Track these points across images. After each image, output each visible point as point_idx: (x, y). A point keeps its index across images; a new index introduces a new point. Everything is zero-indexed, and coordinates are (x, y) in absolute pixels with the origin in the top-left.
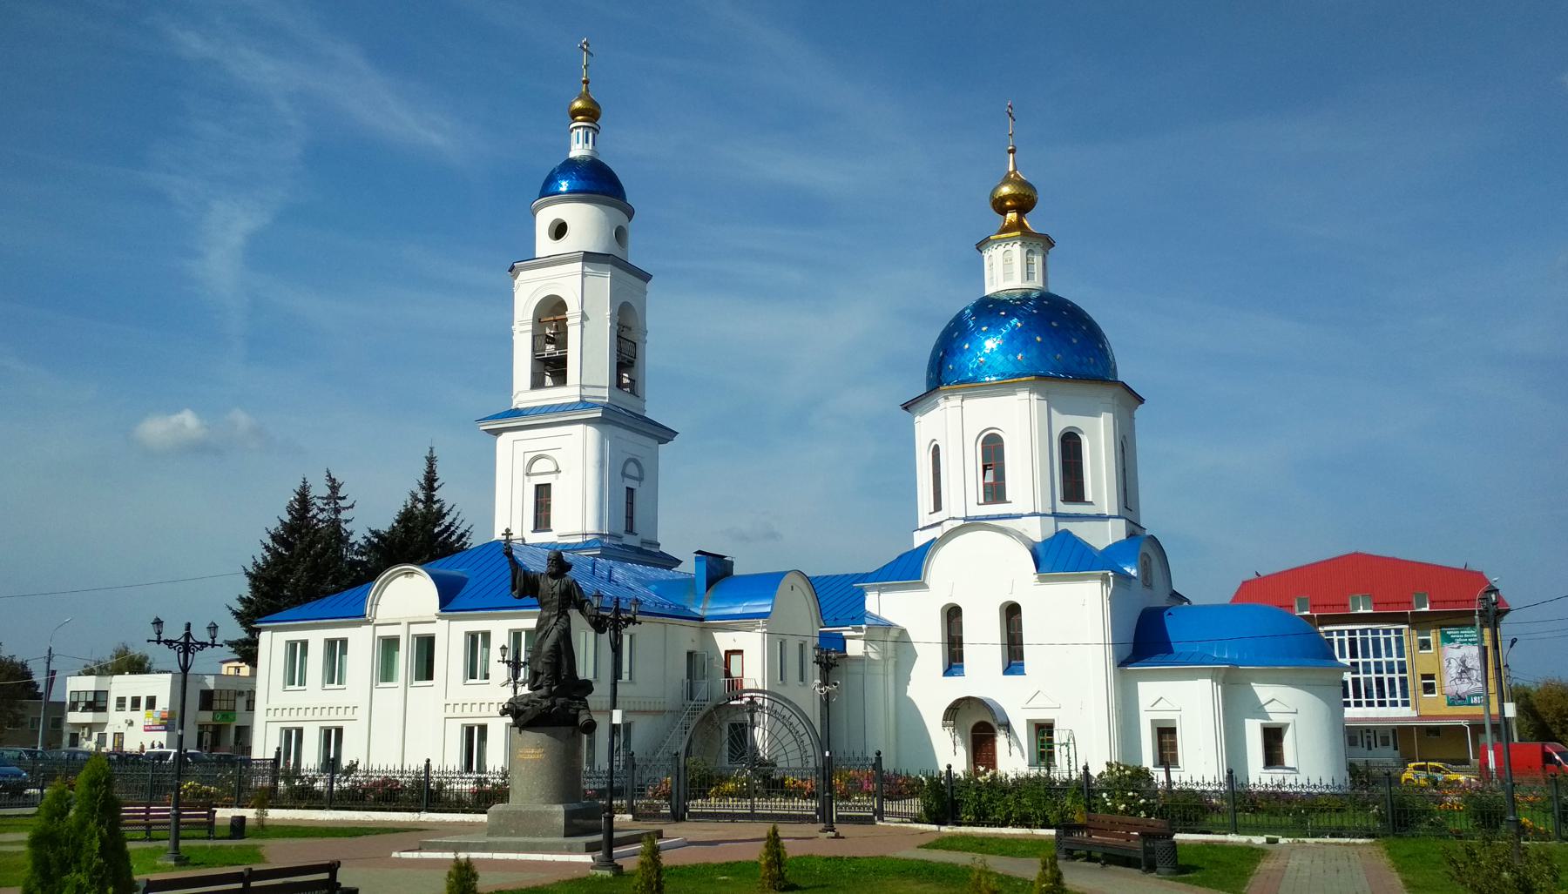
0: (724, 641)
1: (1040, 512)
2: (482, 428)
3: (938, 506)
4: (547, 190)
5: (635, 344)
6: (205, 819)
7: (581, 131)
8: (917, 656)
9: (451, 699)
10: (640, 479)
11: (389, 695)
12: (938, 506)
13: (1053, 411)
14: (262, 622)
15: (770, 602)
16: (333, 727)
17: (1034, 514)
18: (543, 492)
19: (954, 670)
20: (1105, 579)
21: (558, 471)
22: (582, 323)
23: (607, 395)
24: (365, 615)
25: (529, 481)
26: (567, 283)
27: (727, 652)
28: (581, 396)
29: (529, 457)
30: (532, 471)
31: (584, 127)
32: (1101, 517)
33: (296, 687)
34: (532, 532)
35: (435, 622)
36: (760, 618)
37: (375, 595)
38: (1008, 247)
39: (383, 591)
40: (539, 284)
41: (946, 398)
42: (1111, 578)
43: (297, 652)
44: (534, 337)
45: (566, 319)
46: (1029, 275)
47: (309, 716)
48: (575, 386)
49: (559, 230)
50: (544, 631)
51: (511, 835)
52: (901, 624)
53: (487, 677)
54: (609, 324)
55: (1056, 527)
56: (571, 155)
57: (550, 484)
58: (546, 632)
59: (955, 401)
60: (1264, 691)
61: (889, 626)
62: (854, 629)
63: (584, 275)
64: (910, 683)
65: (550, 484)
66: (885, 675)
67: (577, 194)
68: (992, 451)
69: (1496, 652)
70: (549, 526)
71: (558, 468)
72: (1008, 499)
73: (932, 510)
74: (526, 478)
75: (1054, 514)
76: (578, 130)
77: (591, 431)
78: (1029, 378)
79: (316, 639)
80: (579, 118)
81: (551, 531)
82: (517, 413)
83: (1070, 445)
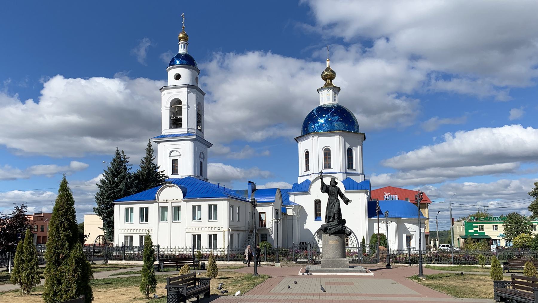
0: (259, 209)
1: (342, 172)
2: (153, 141)
3: (307, 169)
4: (172, 63)
5: (201, 115)
6: (193, 264)
7: (183, 44)
8: (307, 215)
9: (188, 226)
10: (203, 159)
11: (162, 225)
12: (307, 169)
13: (346, 143)
14: (115, 201)
15: (274, 198)
16: (197, 234)
17: (340, 173)
18: (175, 162)
19: (318, 219)
20: (366, 193)
21: (180, 155)
22: (187, 108)
23: (195, 132)
24: (155, 200)
25: (170, 158)
26: (182, 94)
27: (260, 213)
28: (187, 132)
29: (170, 151)
30: (171, 155)
31: (184, 43)
32: (357, 174)
33: (144, 222)
34: (172, 175)
35: (181, 202)
36: (272, 202)
37: (158, 193)
38: (328, 91)
39: (161, 192)
40: (171, 95)
41: (313, 136)
42: (368, 192)
43: (128, 212)
44: (170, 111)
45: (182, 106)
46: (334, 100)
47: (135, 231)
48: (185, 128)
49: (178, 77)
50: (333, 204)
51: (330, 267)
52: (302, 205)
53: (200, 219)
54: (195, 109)
55: (347, 177)
56: (179, 52)
57: (177, 160)
58: (334, 204)
59: (316, 137)
60: (408, 225)
61: (299, 206)
62: (290, 206)
63: (188, 93)
64: (346, 221)
65: (177, 160)
66: (298, 220)
67: (182, 65)
68: (327, 154)
69: (276, 215)
70: (177, 172)
71: (180, 154)
72: (332, 168)
73: (305, 171)
74: (169, 157)
75: (346, 173)
76: (182, 44)
77: (191, 143)
78: (340, 131)
79: (137, 208)
80: (182, 40)
81: (178, 174)
82: (164, 136)
83: (349, 152)
